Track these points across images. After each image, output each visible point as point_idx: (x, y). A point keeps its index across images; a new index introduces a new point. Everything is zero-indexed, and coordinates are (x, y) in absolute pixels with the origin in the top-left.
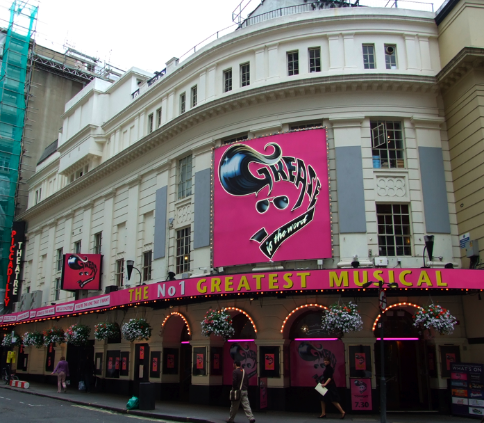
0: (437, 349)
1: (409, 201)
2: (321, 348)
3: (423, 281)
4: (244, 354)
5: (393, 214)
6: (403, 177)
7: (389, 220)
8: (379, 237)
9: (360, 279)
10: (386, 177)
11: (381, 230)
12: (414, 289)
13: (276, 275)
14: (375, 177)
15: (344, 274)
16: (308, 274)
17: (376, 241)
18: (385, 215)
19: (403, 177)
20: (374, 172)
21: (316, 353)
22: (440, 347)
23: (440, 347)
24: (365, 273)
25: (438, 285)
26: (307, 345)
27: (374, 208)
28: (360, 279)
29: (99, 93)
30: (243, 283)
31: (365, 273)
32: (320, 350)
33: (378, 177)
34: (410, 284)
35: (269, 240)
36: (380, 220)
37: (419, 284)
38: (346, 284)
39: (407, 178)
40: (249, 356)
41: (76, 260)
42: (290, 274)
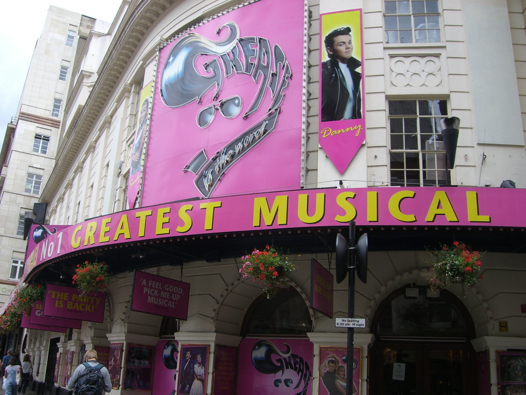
0: (492, 356)
1: (447, 93)
2: (288, 353)
3: (439, 211)
4: (279, 360)
5: (418, 116)
6: (438, 56)
7: (411, 125)
8: (392, 155)
9: (310, 210)
10: (407, 56)
11: (396, 142)
12: (421, 228)
13: (167, 210)
14: (388, 57)
15: (281, 201)
16: (218, 204)
17: (384, 159)
18: (403, 117)
19: (438, 56)
20: (385, 48)
21: (279, 360)
22: (498, 353)
23: (498, 353)
24: (320, 198)
25: (470, 219)
26: (267, 345)
27: (384, 105)
28: (310, 210)
29: (100, 35)
30: (122, 228)
31: (320, 198)
32: (286, 356)
33: (392, 56)
34: (410, 218)
35: (207, 168)
36: (395, 126)
37: (429, 217)
38: (282, 220)
39: (443, 57)
40: (289, 365)
41: (42, 233)
42: (189, 207)
